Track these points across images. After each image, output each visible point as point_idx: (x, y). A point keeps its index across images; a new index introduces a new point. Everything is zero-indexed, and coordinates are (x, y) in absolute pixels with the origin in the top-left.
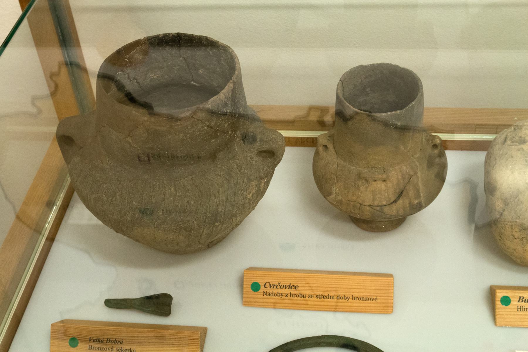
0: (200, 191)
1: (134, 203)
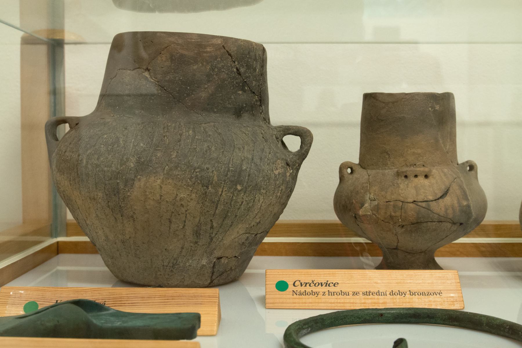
0: (223, 139)
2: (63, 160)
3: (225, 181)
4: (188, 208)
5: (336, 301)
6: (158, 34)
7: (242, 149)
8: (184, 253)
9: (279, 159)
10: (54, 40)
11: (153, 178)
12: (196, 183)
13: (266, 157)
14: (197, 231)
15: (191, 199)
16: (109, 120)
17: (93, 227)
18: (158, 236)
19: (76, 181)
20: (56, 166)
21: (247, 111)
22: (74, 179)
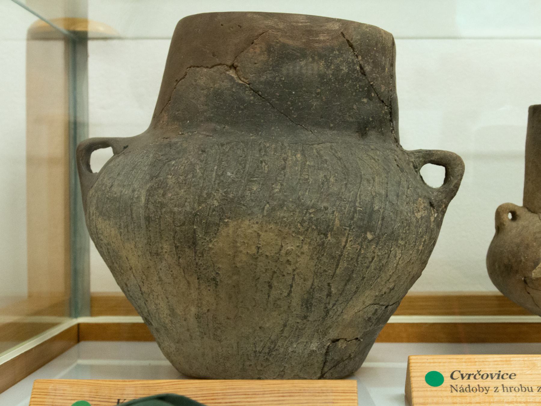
0: (345, 166)
1: (229, 174)
2: (108, 198)
3: (350, 226)
4: (298, 265)
5: (515, 400)
6: (249, 16)
7: (372, 182)
8: (285, 334)
9: (420, 197)
10: (75, 33)
11: (247, 222)
12: (310, 230)
13: (404, 193)
14: (307, 301)
15: (302, 253)
16: (176, 140)
17: (151, 296)
18: (250, 308)
19: (130, 228)
20: (97, 208)
21: (374, 128)
22: (127, 226)
